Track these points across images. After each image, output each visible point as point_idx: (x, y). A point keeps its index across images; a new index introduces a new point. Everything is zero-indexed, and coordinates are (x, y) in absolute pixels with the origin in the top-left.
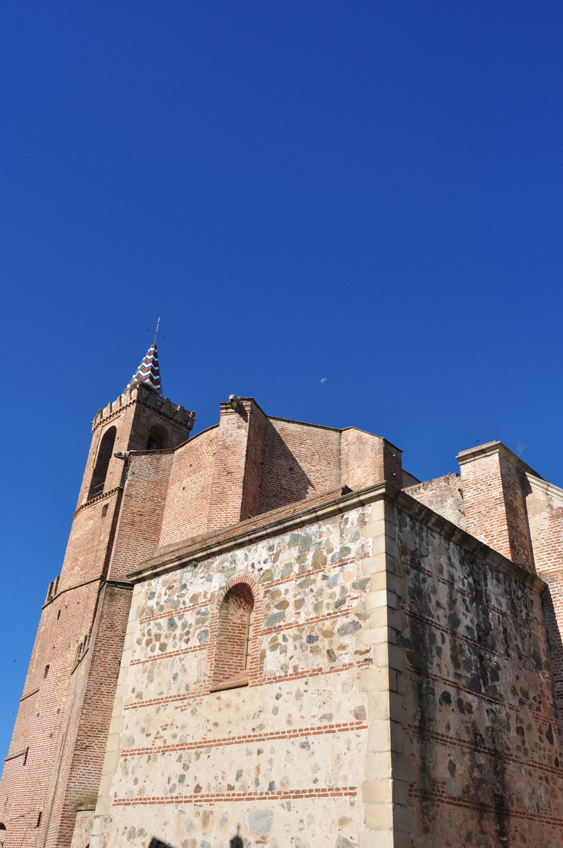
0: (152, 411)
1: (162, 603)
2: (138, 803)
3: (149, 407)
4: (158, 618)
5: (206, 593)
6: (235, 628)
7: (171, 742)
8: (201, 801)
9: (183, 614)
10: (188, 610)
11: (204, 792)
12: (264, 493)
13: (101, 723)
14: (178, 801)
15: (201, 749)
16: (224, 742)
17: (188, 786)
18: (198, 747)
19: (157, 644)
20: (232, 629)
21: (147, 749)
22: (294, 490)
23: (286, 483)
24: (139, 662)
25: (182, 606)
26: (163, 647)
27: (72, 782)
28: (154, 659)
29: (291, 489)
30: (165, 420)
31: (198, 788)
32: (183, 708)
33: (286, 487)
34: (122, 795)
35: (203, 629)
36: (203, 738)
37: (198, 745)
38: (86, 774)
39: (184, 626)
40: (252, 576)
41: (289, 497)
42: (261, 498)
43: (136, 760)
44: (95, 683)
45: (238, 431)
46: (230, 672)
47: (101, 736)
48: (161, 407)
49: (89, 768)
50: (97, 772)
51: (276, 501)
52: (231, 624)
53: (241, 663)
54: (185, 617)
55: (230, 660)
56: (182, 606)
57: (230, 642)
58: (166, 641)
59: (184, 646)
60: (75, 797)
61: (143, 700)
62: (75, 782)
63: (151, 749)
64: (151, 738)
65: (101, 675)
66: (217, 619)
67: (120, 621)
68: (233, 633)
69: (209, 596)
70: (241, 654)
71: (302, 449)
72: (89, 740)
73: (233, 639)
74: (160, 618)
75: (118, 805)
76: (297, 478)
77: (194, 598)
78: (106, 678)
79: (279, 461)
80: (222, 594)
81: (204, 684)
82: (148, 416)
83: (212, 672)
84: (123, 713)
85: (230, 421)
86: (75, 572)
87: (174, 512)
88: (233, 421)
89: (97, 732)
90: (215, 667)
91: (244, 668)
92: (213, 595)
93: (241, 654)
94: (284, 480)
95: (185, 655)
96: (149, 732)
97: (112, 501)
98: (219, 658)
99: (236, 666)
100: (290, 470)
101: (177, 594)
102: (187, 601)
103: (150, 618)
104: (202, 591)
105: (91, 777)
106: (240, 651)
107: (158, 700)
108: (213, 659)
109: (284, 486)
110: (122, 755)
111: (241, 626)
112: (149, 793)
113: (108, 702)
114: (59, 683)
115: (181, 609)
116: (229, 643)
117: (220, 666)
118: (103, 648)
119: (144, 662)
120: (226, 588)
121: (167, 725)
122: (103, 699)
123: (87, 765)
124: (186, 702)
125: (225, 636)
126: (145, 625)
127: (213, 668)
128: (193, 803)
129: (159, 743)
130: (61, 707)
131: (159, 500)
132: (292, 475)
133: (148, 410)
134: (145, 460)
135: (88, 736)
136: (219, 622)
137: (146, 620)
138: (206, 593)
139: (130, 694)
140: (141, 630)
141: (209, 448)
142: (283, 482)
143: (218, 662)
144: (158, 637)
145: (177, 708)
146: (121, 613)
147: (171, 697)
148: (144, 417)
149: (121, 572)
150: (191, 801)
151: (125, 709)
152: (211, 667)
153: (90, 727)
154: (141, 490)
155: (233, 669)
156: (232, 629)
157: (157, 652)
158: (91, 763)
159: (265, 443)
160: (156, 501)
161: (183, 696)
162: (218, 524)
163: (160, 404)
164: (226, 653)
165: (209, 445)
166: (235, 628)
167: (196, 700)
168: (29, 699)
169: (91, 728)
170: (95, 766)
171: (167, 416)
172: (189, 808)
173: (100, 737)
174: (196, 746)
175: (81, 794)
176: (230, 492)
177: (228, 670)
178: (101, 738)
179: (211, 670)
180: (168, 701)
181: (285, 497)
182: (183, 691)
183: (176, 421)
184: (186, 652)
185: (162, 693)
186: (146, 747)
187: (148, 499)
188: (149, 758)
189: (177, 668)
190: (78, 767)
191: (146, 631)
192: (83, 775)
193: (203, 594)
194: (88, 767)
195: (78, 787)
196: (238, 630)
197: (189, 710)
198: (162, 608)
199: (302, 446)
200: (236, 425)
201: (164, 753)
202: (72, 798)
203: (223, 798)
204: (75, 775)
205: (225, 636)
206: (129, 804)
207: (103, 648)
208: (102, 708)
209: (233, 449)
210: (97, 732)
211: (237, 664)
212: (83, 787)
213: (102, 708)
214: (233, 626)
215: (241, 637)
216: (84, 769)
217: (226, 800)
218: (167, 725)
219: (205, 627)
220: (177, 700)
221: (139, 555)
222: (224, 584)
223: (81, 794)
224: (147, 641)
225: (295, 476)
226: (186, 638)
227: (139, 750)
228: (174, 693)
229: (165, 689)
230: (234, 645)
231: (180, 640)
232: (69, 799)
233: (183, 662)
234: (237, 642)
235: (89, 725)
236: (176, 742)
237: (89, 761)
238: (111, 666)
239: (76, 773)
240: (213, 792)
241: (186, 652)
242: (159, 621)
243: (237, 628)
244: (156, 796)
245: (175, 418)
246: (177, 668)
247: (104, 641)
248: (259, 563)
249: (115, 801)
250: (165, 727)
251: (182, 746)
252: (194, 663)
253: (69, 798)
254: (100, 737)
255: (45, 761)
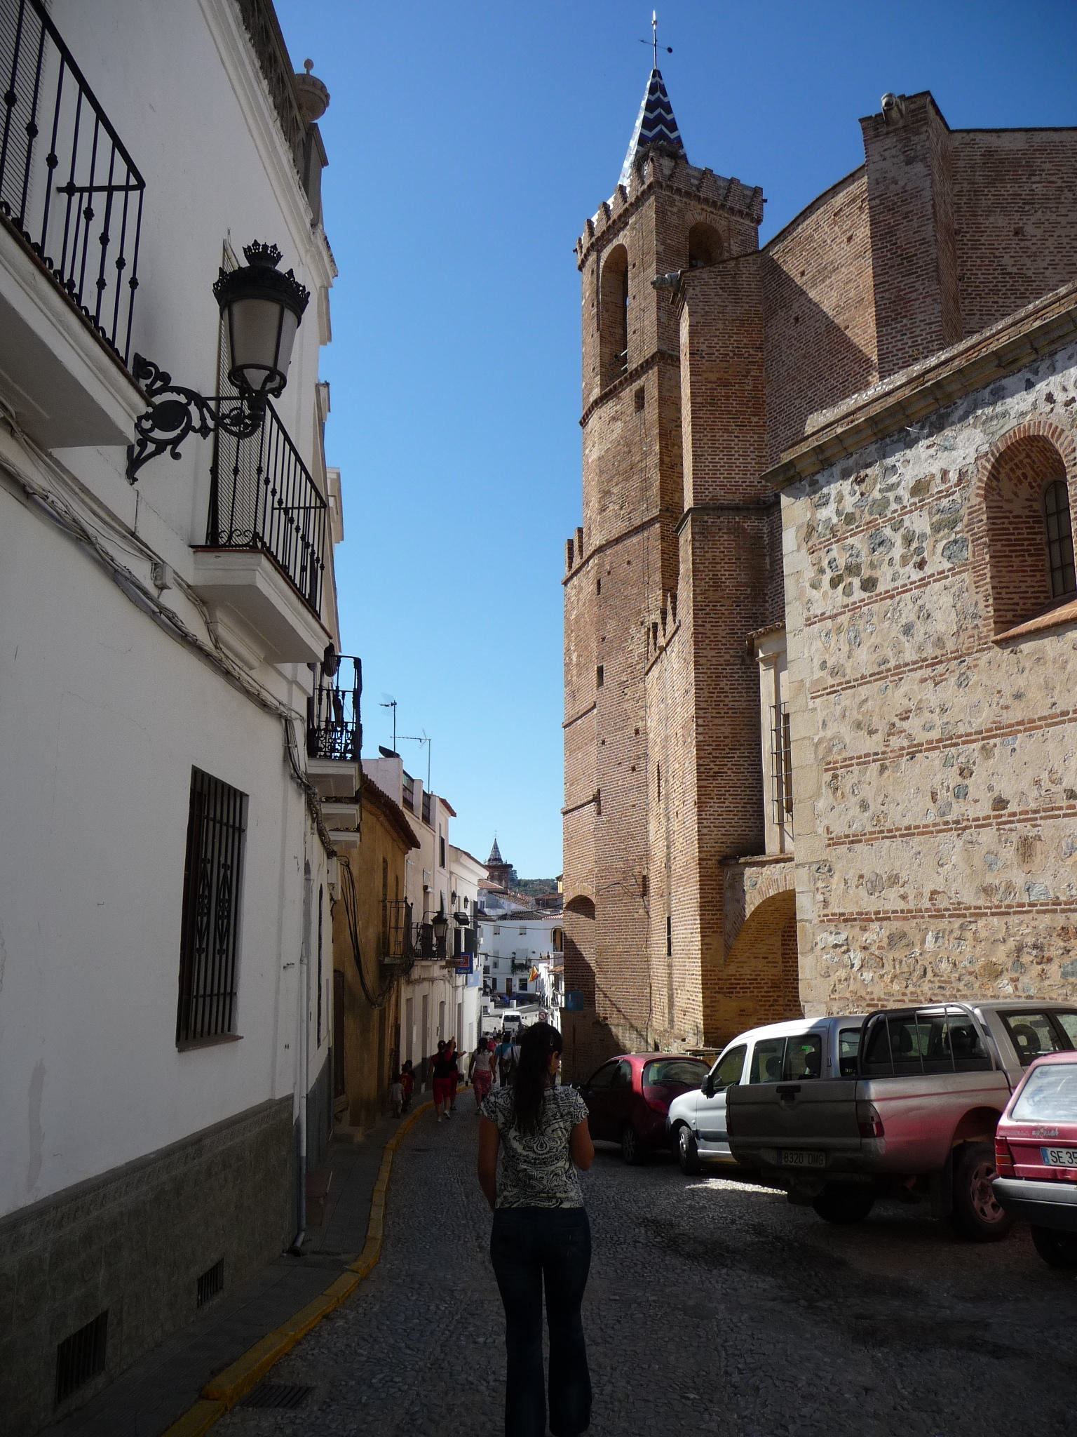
0: (685, 199)
1: (849, 509)
2: (877, 839)
3: (679, 190)
4: (847, 538)
5: (945, 473)
6: (1019, 526)
7: (921, 737)
8: (1012, 822)
9: (902, 520)
10: (911, 511)
11: (1012, 807)
12: (970, 289)
13: (731, 735)
14: (960, 827)
15: (992, 741)
16: (1043, 723)
17: (976, 801)
18: (983, 739)
19: (856, 582)
20: (1014, 529)
21: (876, 754)
22: (1030, 273)
23: (1012, 261)
24: (823, 617)
25: (894, 506)
26: (869, 585)
27: (705, 827)
28: (854, 608)
29: (1024, 271)
30: (712, 213)
31: (1000, 803)
32: (938, 679)
33: (1014, 270)
34: (839, 829)
35: (952, 539)
36: (994, 722)
37: (985, 735)
38: (724, 813)
39: (908, 540)
40: (1053, 419)
41: (1022, 288)
42: (967, 301)
43: (856, 773)
44: (708, 677)
45: (907, 168)
46: (1024, 604)
47: (736, 755)
48: (699, 188)
49: (727, 804)
50: (740, 809)
51: (997, 302)
52: (1012, 520)
53: (1045, 586)
54: (907, 523)
55: (1022, 584)
56: (894, 506)
57: (1016, 551)
58: (875, 574)
59: (916, 575)
60: (714, 847)
61: (847, 678)
62: (709, 827)
63: (884, 753)
64: (879, 737)
65: (714, 663)
66: (983, 513)
67: (727, 573)
68: (1019, 534)
69: (954, 477)
70: (1041, 571)
71: (1034, 186)
72: (718, 763)
73: (1019, 545)
74: (851, 536)
75: (834, 844)
76: (1034, 249)
77: (919, 488)
78: (724, 667)
79: (992, 219)
80: (984, 468)
81: (976, 632)
82: (680, 211)
83: (991, 609)
84: (811, 705)
85: (886, 154)
86: (608, 513)
87: (785, 368)
88: (893, 152)
89: (728, 751)
90: (995, 599)
91: (1051, 594)
92: (962, 475)
93: (1041, 571)
94: (1007, 256)
95: (922, 590)
96: (873, 727)
97: (650, 382)
98: (1000, 582)
99: (1034, 592)
100: (1016, 234)
101: (878, 487)
102: (906, 496)
103: (829, 539)
104: (935, 468)
105: (732, 817)
106: (1037, 566)
107: (878, 673)
108: (989, 586)
109: (1010, 269)
110: (827, 770)
111: (1031, 520)
112: (896, 817)
113: (736, 703)
114: (626, 691)
115: (895, 511)
116: (1013, 554)
117: (1004, 596)
118: (708, 620)
119: (833, 617)
120: (993, 454)
121: (910, 711)
122: (726, 699)
123: (722, 800)
124: (940, 668)
125: (1004, 542)
126: (822, 553)
127: (991, 601)
128: (995, 827)
129: (896, 742)
130: (640, 724)
131: (752, 352)
132: (1022, 244)
133: (677, 197)
134: (711, 281)
135: (713, 757)
136: (988, 518)
137: (822, 546)
138: (945, 473)
139: (818, 674)
140: (814, 565)
141: (836, 228)
142: (1007, 260)
143: (999, 590)
144: (852, 569)
145: (923, 681)
146: (726, 558)
147: (907, 665)
148: (673, 214)
149: (711, 490)
150: (990, 825)
151: (812, 698)
152: (987, 601)
153: (714, 744)
154: (716, 339)
155: (1030, 598)
156: (1014, 529)
157: (858, 594)
158: (728, 796)
159: (957, 187)
160: (746, 355)
161: (932, 659)
162: (901, 361)
163: (696, 182)
164: (1011, 571)
165: (835, 223)
166: (1019, 526)
167: (964, 661)
168: (579, 722)
169: (716, 745)
170: (734, 801)
171: (714, 204)
172: (987, 837)
173: (734, 757)
174: (980, 736)
175: (722, 843)
176: (914, 296)
177: (1021, 602)
178: (736, 759)
179: (987, 606)
180: (904, 672)
181: (1014, 291)
182: (930, 652)
183: (732, 209)
184: (923, 583)
185: (885, 661)
186: (872, 752)
187: (731, 354)
188: (883, 768)
189: (908, 613)
190: (709, 805)
191: (825, 564)
192: (719, 815)
193: (938, 476)
194: (724, 803)
195: (715, 833)
196: (1027, 528)
197: (953, 680)
198: (850, 519)
199: (1034, 179)
200: (902, 158)
201: (912, 756)
202: (709, 849)
203: (1061, 812)
204: (708, 817)
205: (1004, 542)
206: (860, 841)
207: (708, 620)
208: (728, 713)
209: (905, 209)
210: (728, 751)
211: (1036, 589)
212: (724, 832)
213: (728, 713)
214: (1014, 523)
215: (1035, 539)
216: (718, 807)
217: (1065, 816)
218: (910, 711)
219: (957, 533)
220: (921, 668)
221: (736, 456)
222: (985, 448)
223: (722, 843)
224: (832, 580)
225: (1028, 243)
226: (916, 559)
227: (860, 757)
228: (910, 655)
229: (889, 653)
230: (1023, 556)
231: (904, 565)
232: (705, 851)
233: (920, 602)
234: (1028, 550)
235: (713, 741)
236: (935, 735)
237: (725, 795)
238: (728, 646)
239: (708, 813)
240: (1033, 806)
241: (923, 583)
242: (850, 541)
243: (1023, 525)
244: (913, 824)
245: (729, 204)
246: (908, 613)
247: (708, 608)
248: (1065, 389)
249: (829, 839)
250: (904, 715)
251: (949, 740)
252: (947, 600)
253: (705, 849)
254: (734, 757)
255: (634, 806)
